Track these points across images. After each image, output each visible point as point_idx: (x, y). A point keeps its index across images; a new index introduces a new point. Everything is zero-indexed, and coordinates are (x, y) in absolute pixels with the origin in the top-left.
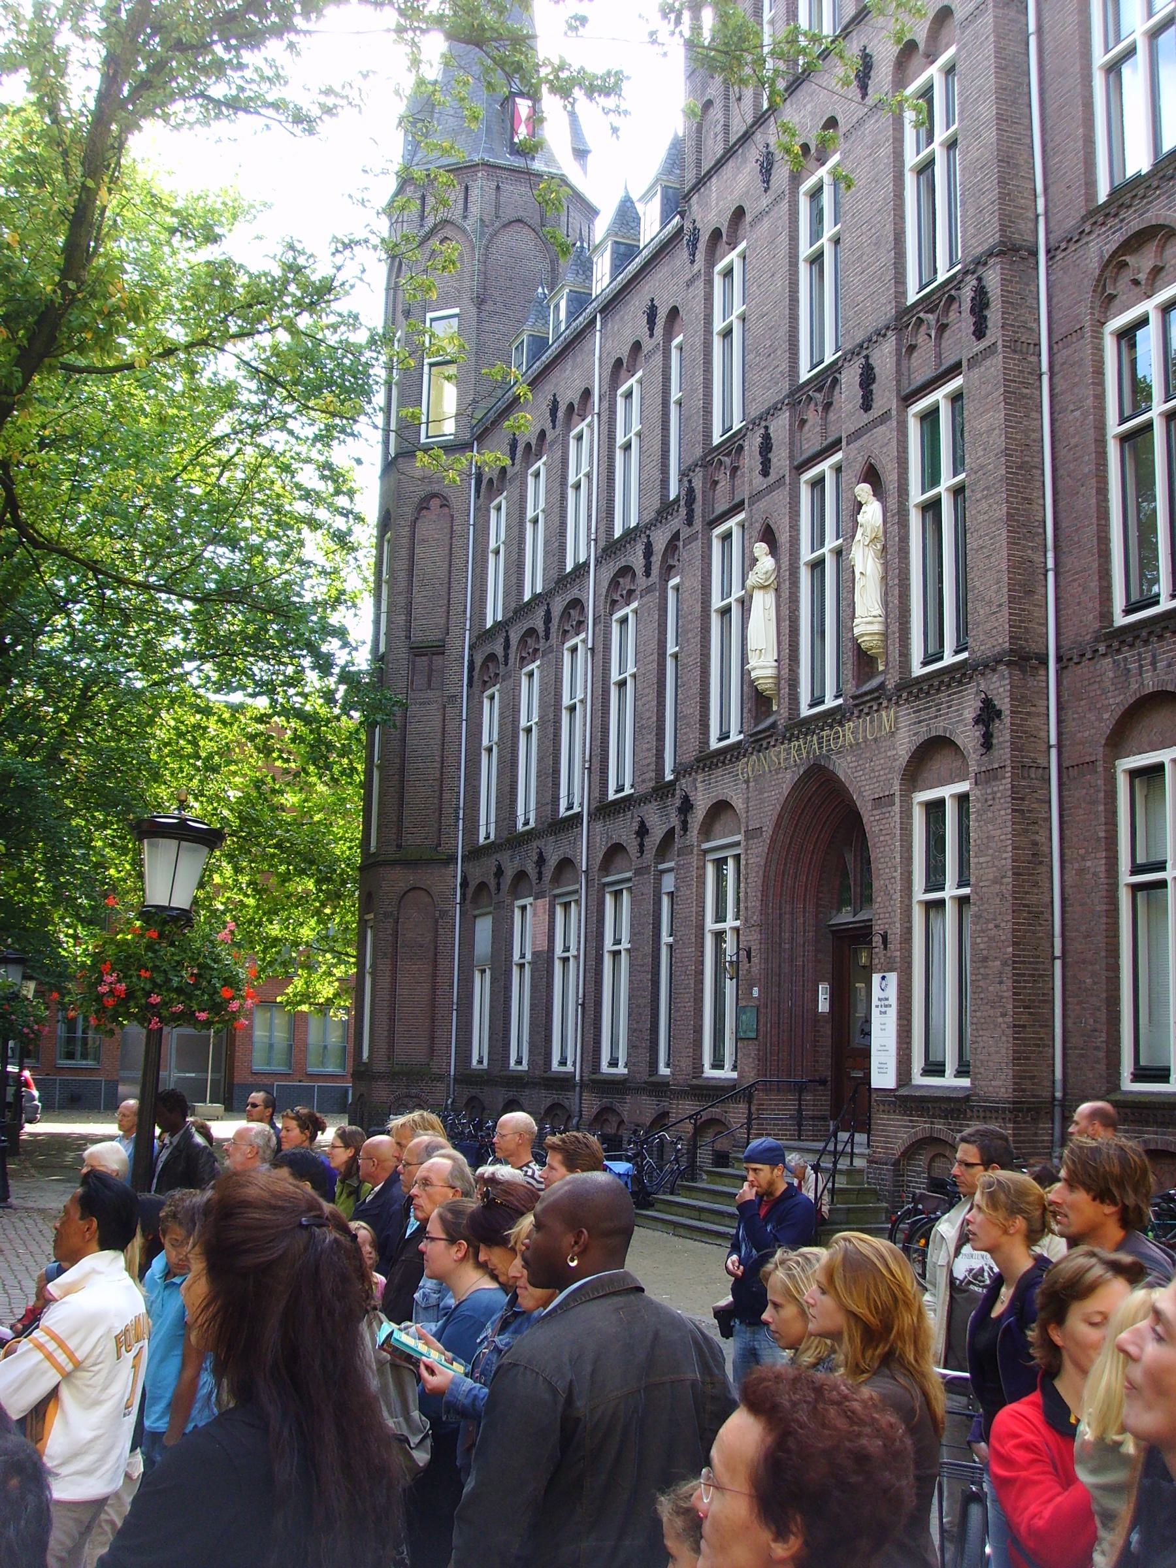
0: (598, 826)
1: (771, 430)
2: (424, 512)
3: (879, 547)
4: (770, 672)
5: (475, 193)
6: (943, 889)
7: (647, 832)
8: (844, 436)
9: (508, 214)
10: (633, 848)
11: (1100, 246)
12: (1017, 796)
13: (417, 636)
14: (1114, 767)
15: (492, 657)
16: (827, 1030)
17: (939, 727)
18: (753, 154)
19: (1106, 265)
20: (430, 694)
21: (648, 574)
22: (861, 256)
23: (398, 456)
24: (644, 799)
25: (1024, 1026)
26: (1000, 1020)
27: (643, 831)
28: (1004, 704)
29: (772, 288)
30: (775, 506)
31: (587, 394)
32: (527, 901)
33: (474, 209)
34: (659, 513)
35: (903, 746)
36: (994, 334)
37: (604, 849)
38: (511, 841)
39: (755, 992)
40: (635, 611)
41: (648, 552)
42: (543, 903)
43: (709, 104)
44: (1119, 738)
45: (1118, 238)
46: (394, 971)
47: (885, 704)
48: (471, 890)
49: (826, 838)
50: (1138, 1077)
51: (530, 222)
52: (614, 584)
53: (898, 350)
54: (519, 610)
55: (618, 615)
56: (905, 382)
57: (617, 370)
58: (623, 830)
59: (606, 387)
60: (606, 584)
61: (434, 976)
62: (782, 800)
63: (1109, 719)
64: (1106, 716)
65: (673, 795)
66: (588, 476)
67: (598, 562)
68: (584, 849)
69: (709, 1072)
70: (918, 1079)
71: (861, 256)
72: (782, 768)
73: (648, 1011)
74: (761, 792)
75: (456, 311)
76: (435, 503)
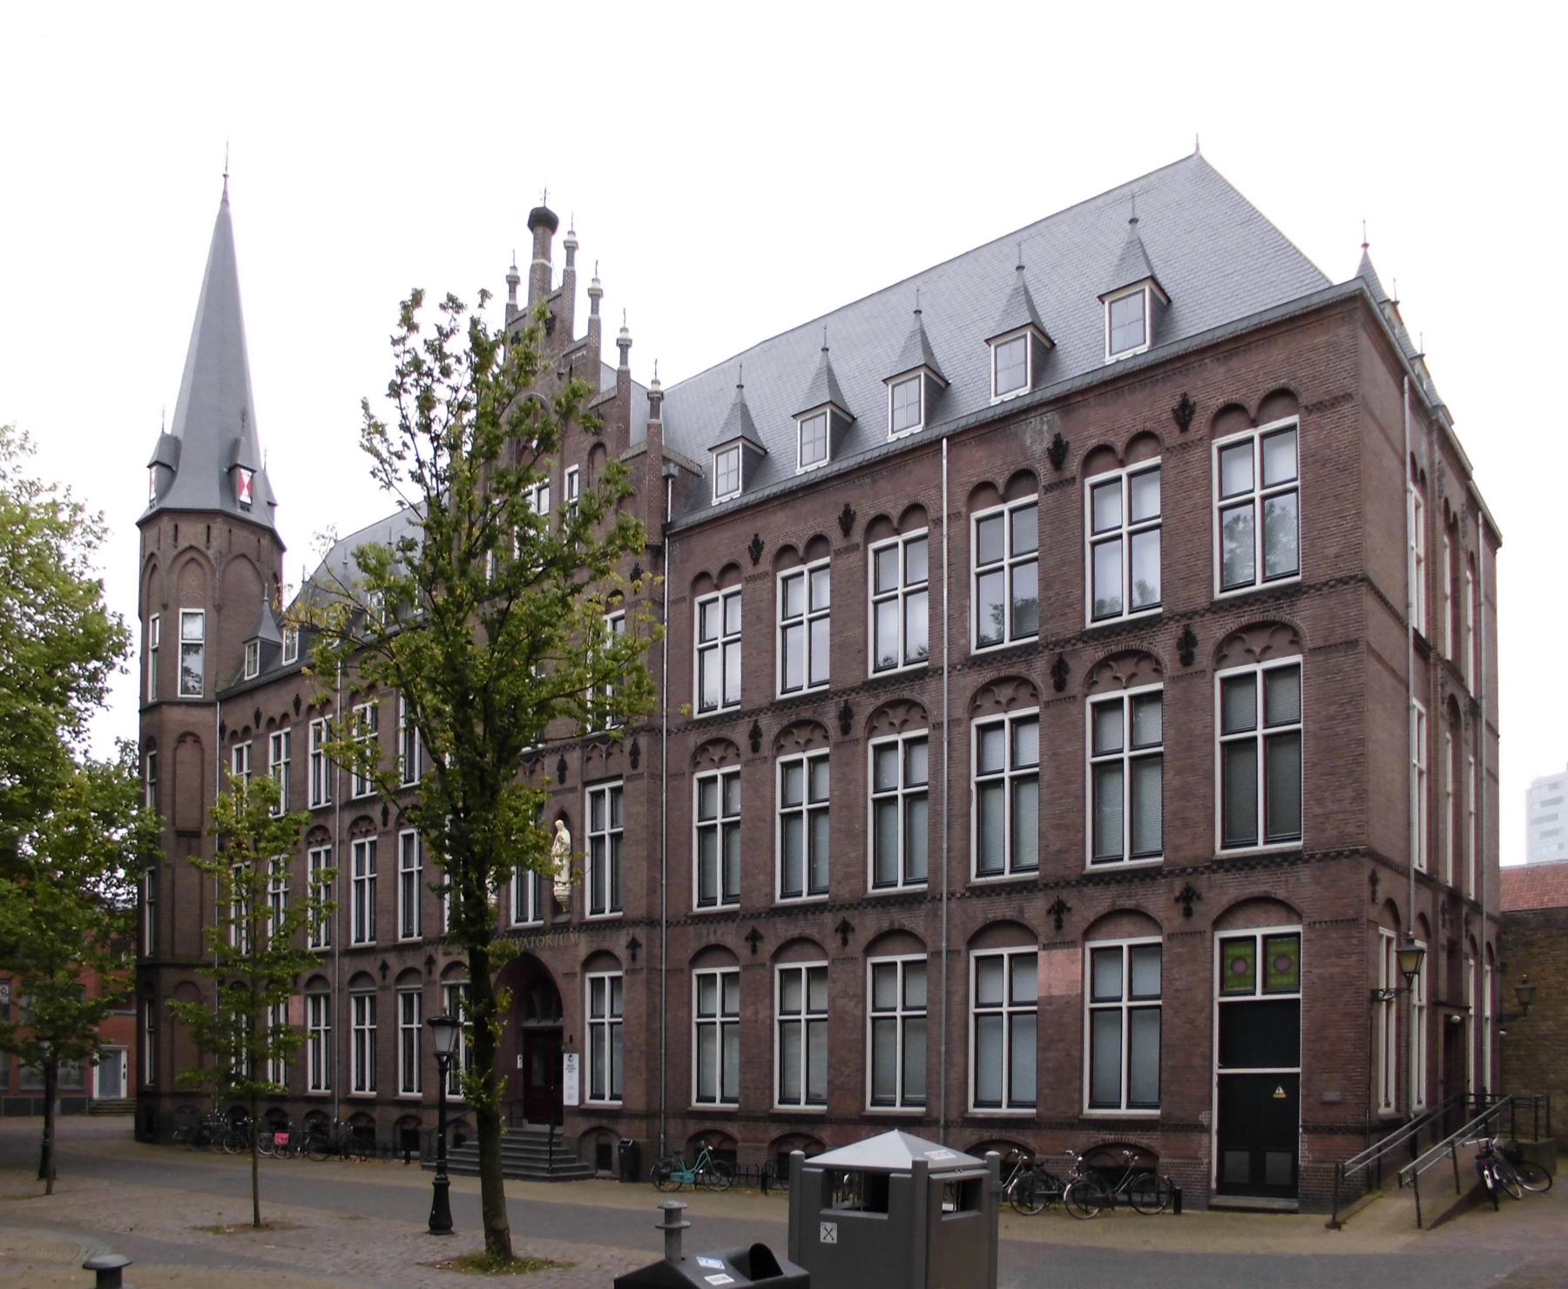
0: (346, 961)
5: (215, 532)
9: (237, 550)
11: (694, 739)
12: (648, 982)
13: (180, 825)
16: (521, 1077)
17: (605, 945)
21: (385, 824)
28: (643, 940)
33: (214, 544)
36: (642, 768)
44: (695, 961)
45: (706, 737)
46: (173, 1033)
50: (698, 1100)
52: (355, 823)
58: (370, 965)
63: (691, 953)
69: (401, 1093)
70: (588, 1101)
76: (189, 739)
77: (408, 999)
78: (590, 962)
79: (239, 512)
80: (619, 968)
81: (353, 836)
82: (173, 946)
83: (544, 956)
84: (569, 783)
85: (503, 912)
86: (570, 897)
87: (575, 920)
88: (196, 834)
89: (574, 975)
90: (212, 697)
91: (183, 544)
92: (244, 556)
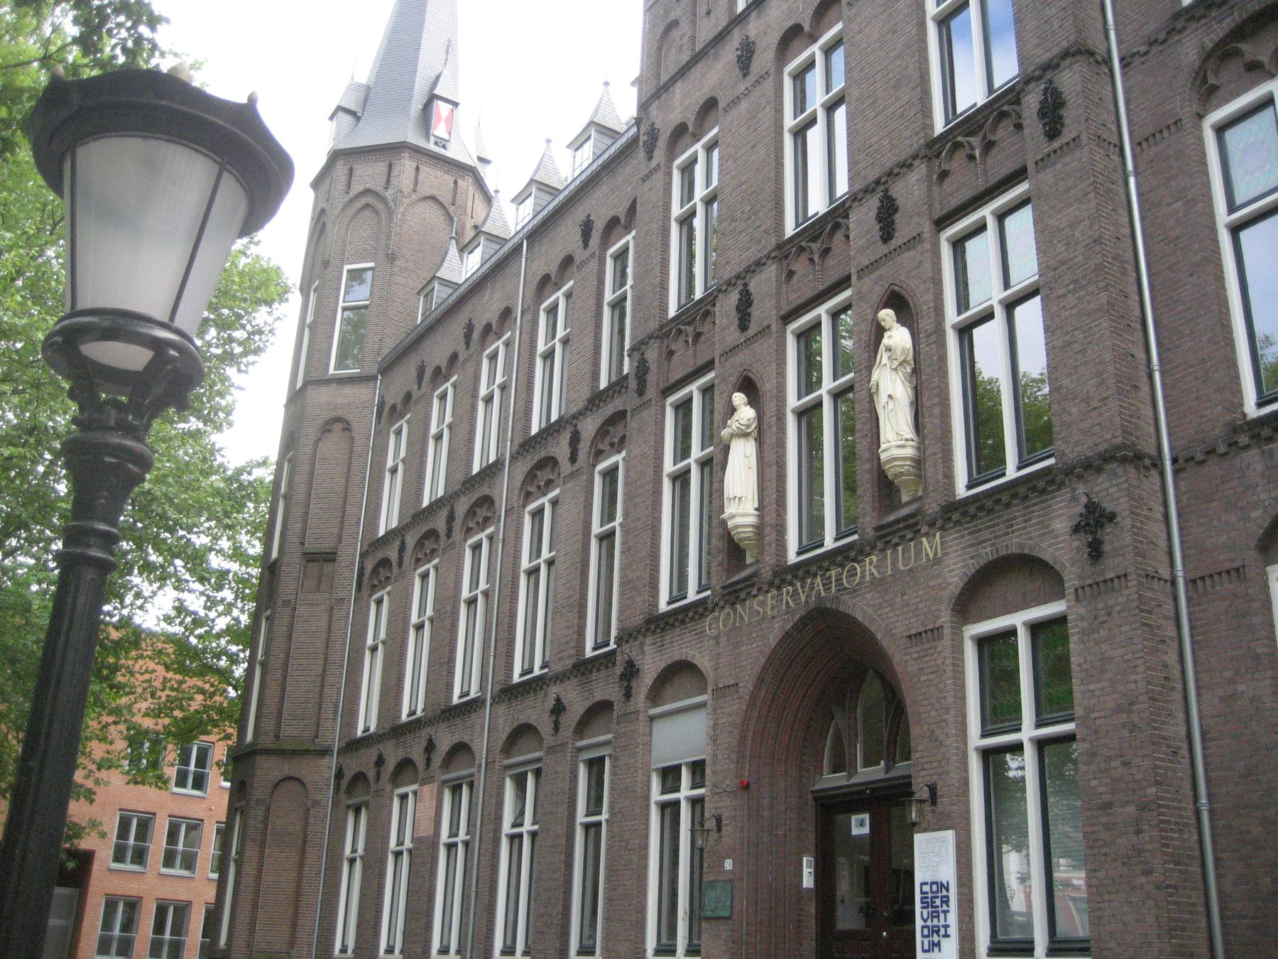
0: (502, 709)
1: (752, 287)
2: (327, 434)
3: (909, 370)
4: (752, 520)
6: (1019, 730)
7: (564, 709)
8: (853, 271)
9: (425, 190)
10: (545, 728)
13: (311, 546)
14: (1266, 574)
15: (385, 563)
17: (1014, 543)
18: (730, 51)
19: (1209, 56)
20: (319, 596)
21: (573, 459)
22: (875, 101)
23: (305, 384)
24: (560, 678)
25: (1175, 887)
26: (1143, 880)
27: (559, 709)
29: (752, 158)
30: (755, 358)
31: (507, 313)
32: (409, 789)
34: (590, 401)
35: (955, 572)
37: (508, 730)
38: (396, 731)
39: (728, 865)
40: (555, 503)
41: (575, 440)
42: (428, 791)
43: (674, 24)
47: (925, 529)
48: (345, 782)
49: (834, 684)
51: (442, 200)
52: (531, 476)
53: (929, 177)
54: (415, 516)
55: (533, 506)
56: (937, 205)
57: (545, 284)
58: (535, 711)
59: (529, 302)
60: (520, 477)
61: (301, 864)
62: (768, 652)
64: (1254, 514)
65: (614, 664)
66: (503, 388)
67: (513, 458)
68: (484, 734)
71: (875, 101)
72: (771, 617)
73: (560, 894)
74: (741, 648)
75: (372, 265)
77: (596, 765)
78: (975, 594)
79: (431, 146)
80: (1059, 594)
81: (528, 497)
82: (279, 724)
83: (862, 608)
84: (904, 231)
85: (770, 537)
86: (919, 462)
87: (932, 506)
88: (329, 557)
89: (936, 632)
90: (374, 369)
91: (357, 188)
92: (433, 198)
